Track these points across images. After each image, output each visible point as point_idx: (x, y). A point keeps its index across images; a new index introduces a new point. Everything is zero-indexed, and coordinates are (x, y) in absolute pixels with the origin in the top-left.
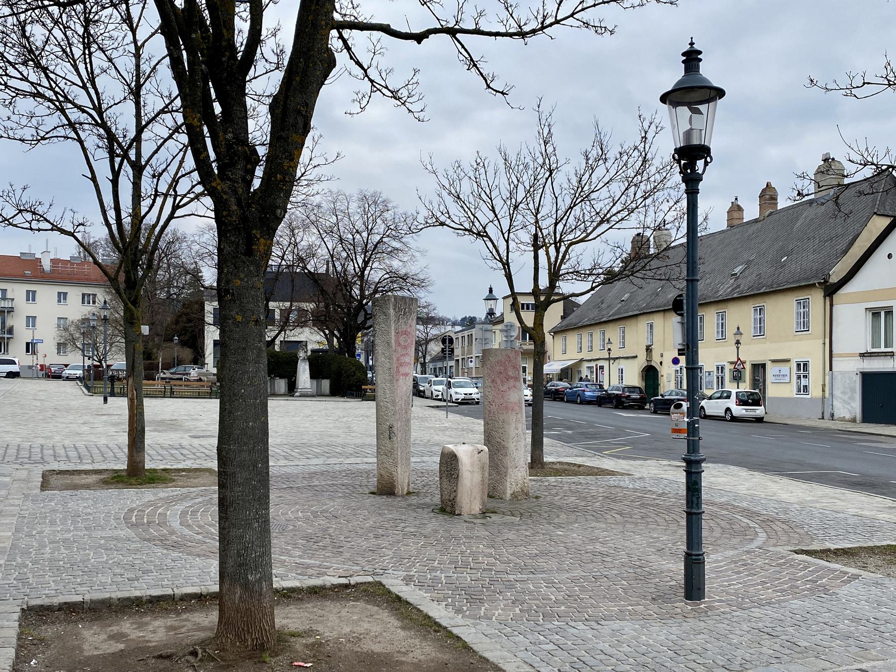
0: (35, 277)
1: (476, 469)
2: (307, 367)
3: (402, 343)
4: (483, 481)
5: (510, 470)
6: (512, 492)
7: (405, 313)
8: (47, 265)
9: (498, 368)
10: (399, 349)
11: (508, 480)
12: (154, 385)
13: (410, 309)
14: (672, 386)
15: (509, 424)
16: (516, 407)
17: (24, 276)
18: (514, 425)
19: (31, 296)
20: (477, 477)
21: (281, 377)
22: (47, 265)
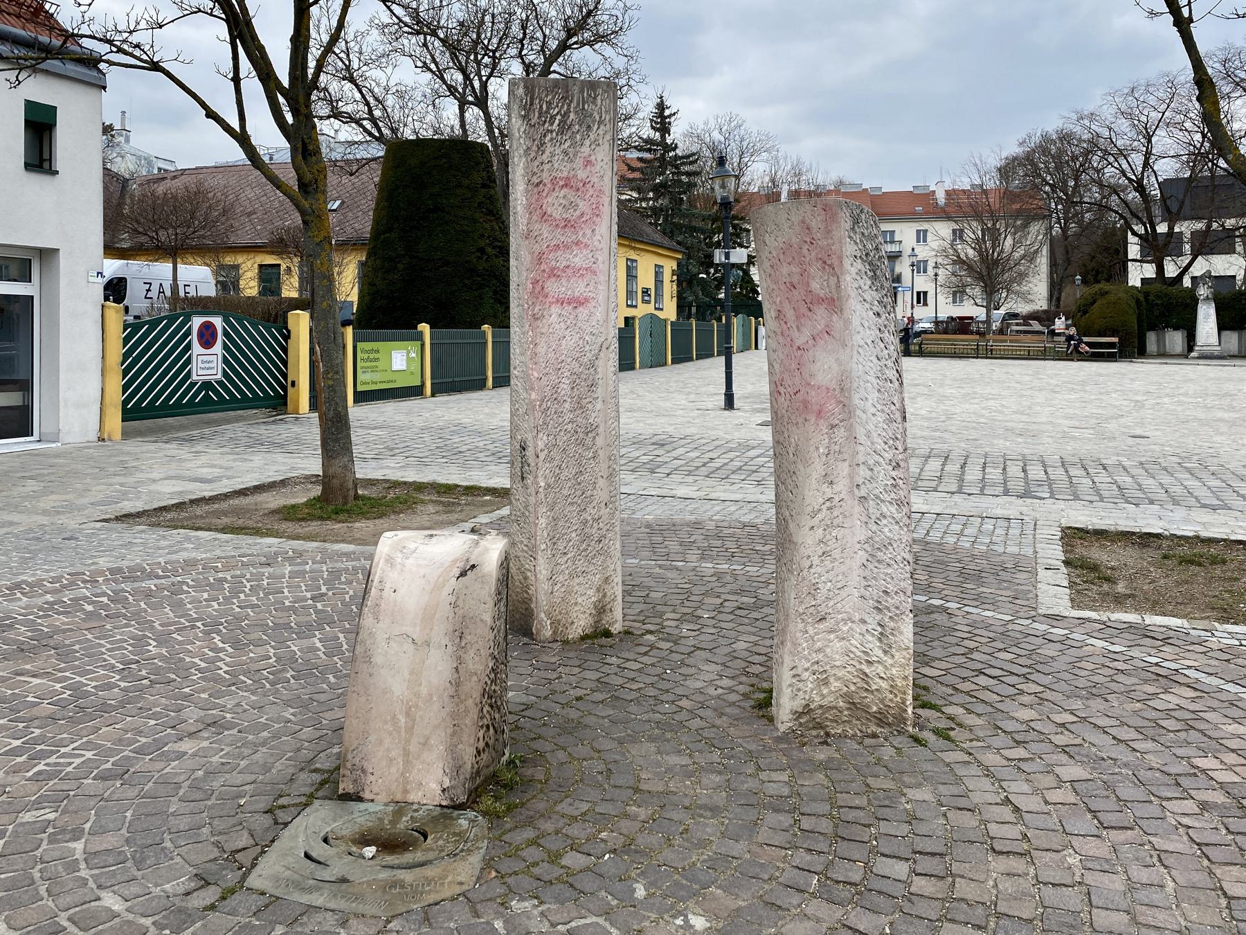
0: (926, 213)
1: (440, 633)
2: (1212, 311)
3: (556, 213)
4: (457, 684)
5: (795, 627)
6: (798, 704)
7: (564, 127)
8: (941, 197)
9: (785, 270)
10: (545, 230)
11: (788, 661)
12: (1005, 341)
13: (584, 116)
14: (735, 320)
15: (807, 463)
16: (830, 406)
17: (915, 213)
18: (817, 469)
19: (922, 236)
20: (438, 668)
21: (1176, 328)
22: (941, 197)
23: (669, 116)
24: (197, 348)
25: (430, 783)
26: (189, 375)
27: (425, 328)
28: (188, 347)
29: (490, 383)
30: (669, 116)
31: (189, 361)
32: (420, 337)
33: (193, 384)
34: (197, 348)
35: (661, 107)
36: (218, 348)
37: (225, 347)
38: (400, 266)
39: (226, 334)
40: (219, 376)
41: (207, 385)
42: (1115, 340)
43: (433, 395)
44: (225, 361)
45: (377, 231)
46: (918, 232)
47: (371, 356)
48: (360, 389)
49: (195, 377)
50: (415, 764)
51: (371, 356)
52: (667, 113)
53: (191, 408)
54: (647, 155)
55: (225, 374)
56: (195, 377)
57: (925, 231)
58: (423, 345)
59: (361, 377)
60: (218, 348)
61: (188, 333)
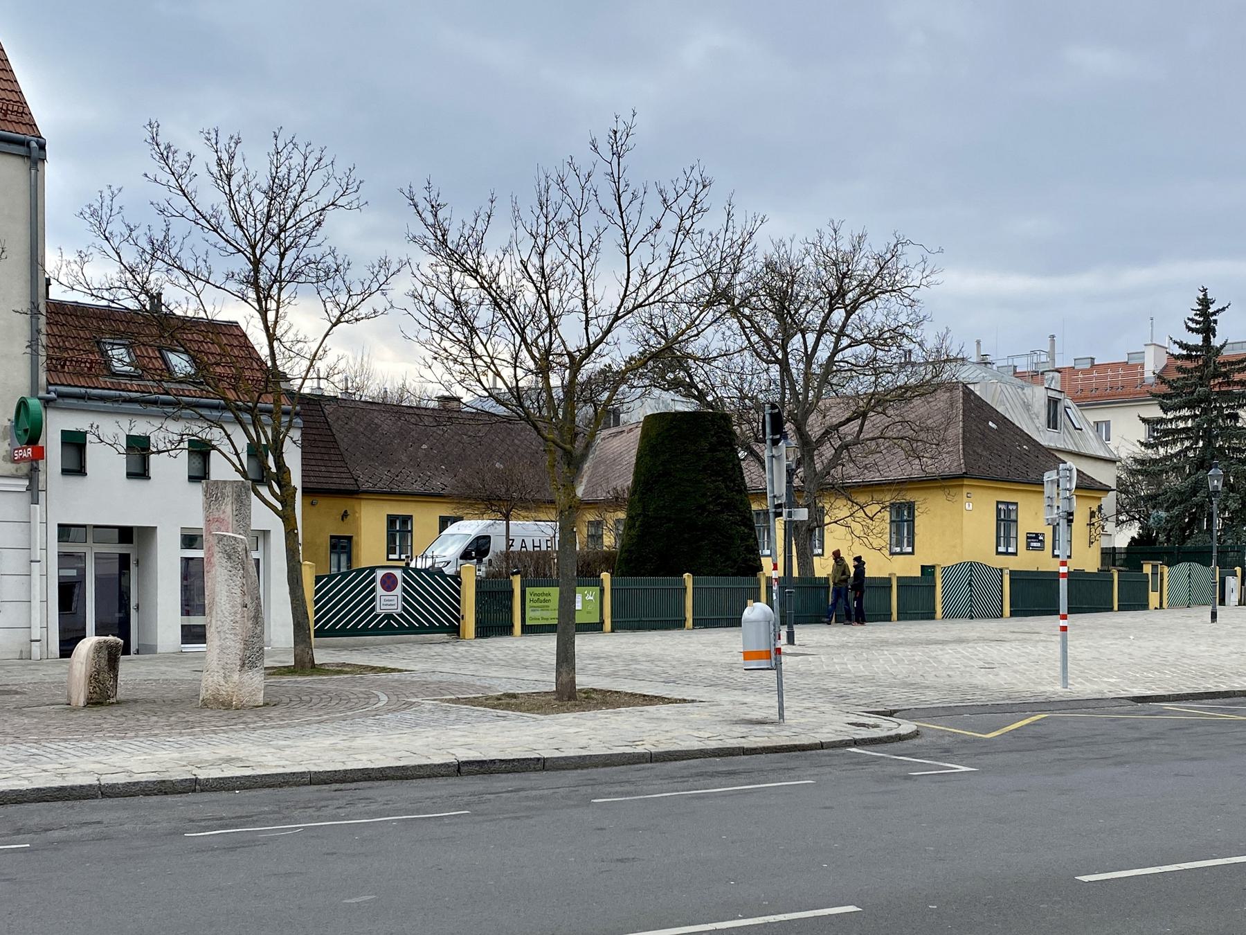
23: (1214, 314)
24: (380, 591)
25: (81, 704)
26: (373, 609)
27: (688, 577)
28: (373, 590)
29: (689, 622)
30: (1214, 314)
31: (373, 600)
32: (599, 583)
33: (377, 616)
34: (380, 591)
35: (1205, 302)
36: (398, 590)
37: (404, 590)
38: (637, 524)
39: (405, 581)
40: (399, 610)
41: (389, 616)
42: (795, 574)
43: (613, 631)
44: (404, 599)
45: (633, 491)
46: (392, 520)
47: (542, 598)
48: (528, 622)
49: (378, 611)
50: (80, 698)
51: (542, 598)
52: (1212, 309)
53: (376, 631)
54: (1189, 365)
55: (404, 609)
56: (378, 611)
57: (406, 520)
58: (602, 591)
59: (529, 614)
60: (398, 590)
61: (373, 580)
